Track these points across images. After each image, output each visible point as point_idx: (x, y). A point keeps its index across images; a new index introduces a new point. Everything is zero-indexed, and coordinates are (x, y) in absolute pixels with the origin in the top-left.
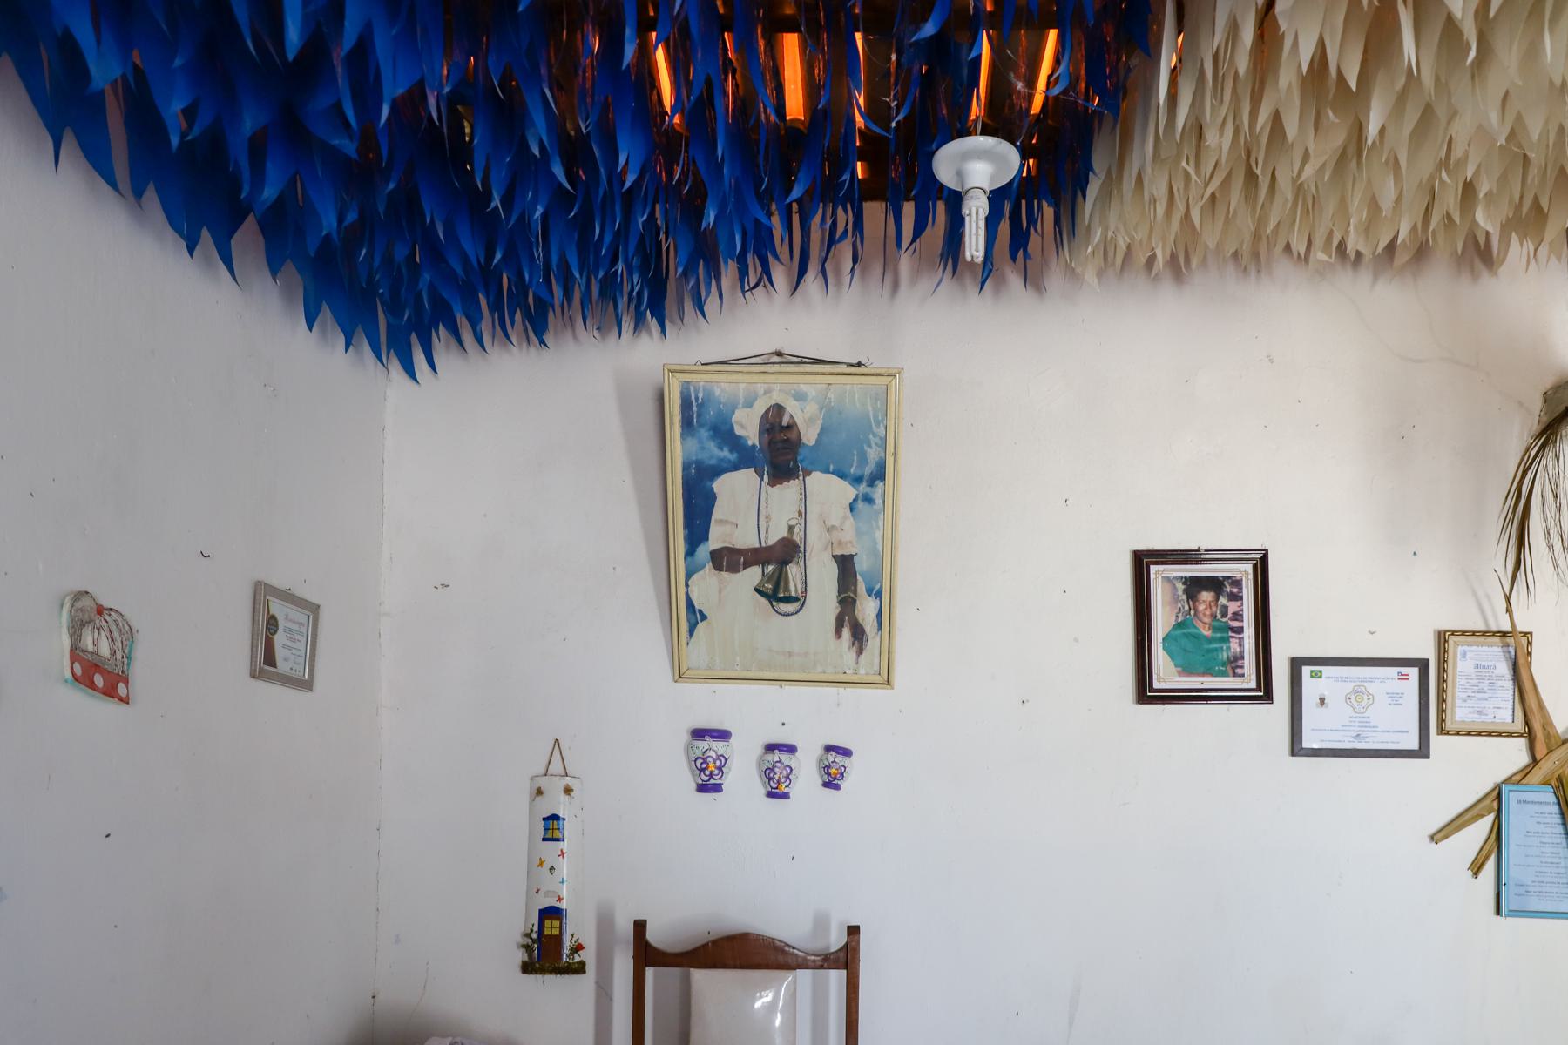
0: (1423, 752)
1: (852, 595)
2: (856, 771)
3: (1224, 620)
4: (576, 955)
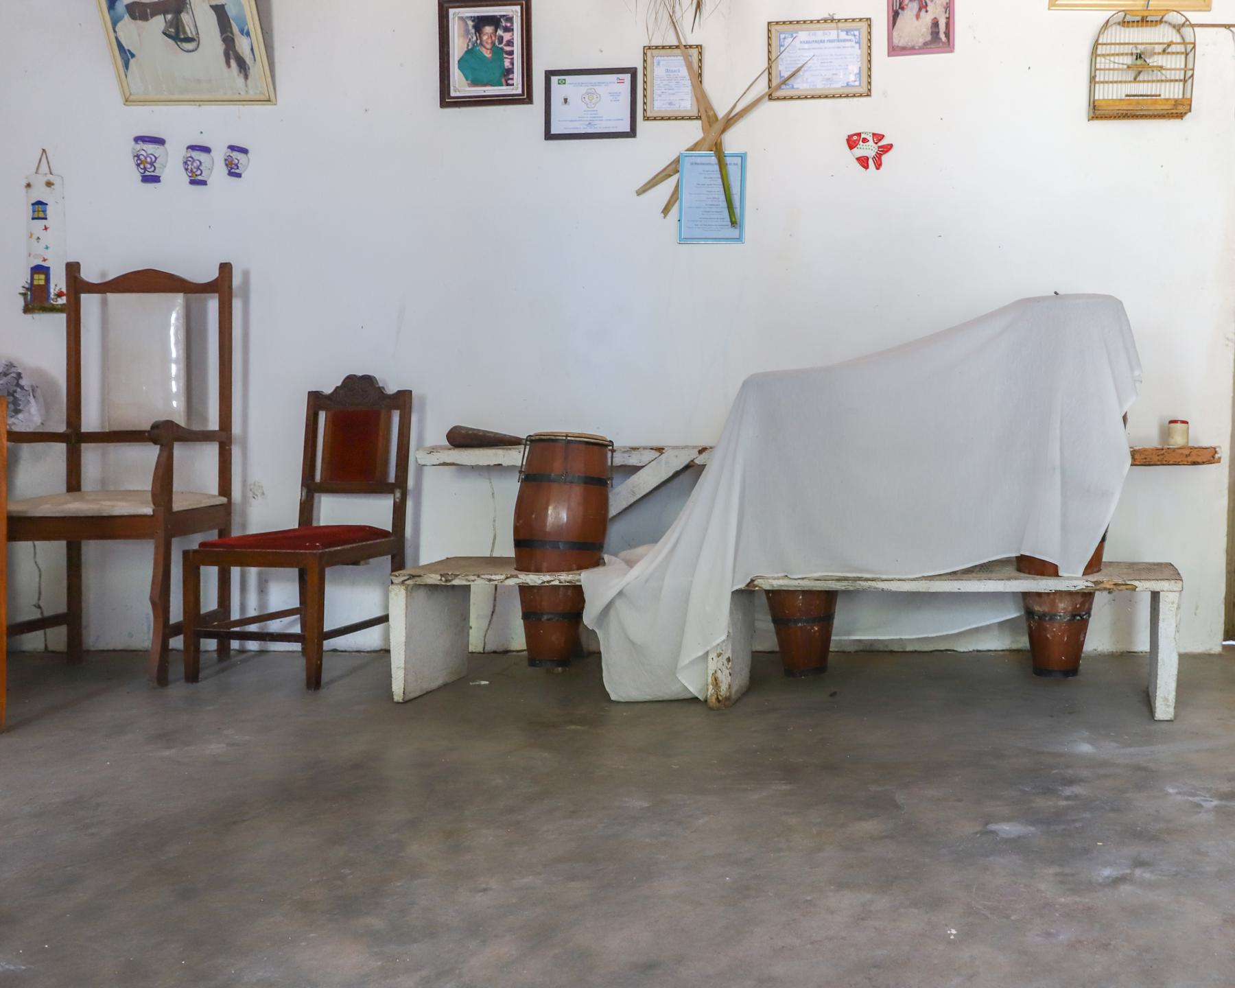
0: (632, 133)
1: (230, 35)
2: (251, 166)
3: (500, 46)
4: (59, 299)
